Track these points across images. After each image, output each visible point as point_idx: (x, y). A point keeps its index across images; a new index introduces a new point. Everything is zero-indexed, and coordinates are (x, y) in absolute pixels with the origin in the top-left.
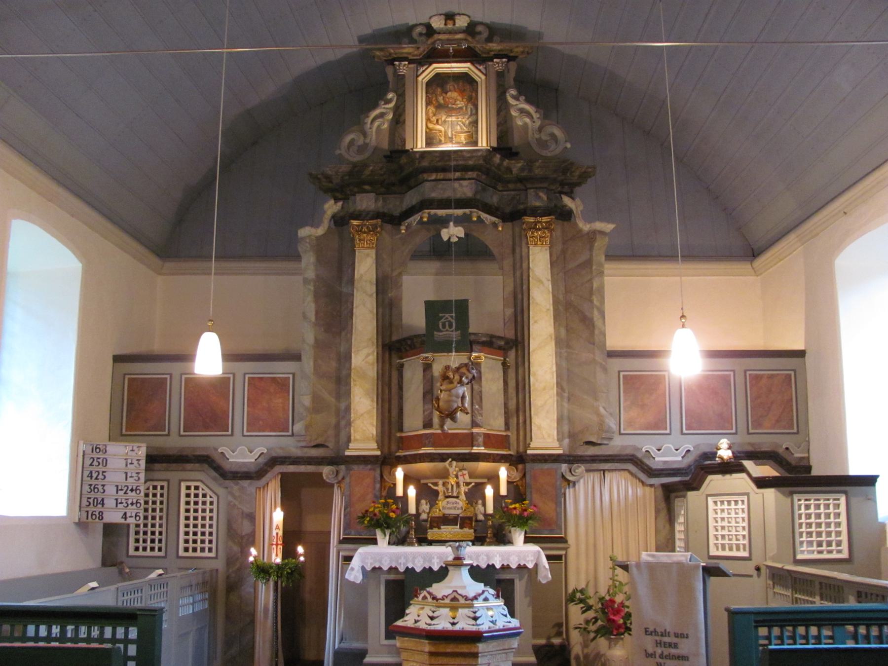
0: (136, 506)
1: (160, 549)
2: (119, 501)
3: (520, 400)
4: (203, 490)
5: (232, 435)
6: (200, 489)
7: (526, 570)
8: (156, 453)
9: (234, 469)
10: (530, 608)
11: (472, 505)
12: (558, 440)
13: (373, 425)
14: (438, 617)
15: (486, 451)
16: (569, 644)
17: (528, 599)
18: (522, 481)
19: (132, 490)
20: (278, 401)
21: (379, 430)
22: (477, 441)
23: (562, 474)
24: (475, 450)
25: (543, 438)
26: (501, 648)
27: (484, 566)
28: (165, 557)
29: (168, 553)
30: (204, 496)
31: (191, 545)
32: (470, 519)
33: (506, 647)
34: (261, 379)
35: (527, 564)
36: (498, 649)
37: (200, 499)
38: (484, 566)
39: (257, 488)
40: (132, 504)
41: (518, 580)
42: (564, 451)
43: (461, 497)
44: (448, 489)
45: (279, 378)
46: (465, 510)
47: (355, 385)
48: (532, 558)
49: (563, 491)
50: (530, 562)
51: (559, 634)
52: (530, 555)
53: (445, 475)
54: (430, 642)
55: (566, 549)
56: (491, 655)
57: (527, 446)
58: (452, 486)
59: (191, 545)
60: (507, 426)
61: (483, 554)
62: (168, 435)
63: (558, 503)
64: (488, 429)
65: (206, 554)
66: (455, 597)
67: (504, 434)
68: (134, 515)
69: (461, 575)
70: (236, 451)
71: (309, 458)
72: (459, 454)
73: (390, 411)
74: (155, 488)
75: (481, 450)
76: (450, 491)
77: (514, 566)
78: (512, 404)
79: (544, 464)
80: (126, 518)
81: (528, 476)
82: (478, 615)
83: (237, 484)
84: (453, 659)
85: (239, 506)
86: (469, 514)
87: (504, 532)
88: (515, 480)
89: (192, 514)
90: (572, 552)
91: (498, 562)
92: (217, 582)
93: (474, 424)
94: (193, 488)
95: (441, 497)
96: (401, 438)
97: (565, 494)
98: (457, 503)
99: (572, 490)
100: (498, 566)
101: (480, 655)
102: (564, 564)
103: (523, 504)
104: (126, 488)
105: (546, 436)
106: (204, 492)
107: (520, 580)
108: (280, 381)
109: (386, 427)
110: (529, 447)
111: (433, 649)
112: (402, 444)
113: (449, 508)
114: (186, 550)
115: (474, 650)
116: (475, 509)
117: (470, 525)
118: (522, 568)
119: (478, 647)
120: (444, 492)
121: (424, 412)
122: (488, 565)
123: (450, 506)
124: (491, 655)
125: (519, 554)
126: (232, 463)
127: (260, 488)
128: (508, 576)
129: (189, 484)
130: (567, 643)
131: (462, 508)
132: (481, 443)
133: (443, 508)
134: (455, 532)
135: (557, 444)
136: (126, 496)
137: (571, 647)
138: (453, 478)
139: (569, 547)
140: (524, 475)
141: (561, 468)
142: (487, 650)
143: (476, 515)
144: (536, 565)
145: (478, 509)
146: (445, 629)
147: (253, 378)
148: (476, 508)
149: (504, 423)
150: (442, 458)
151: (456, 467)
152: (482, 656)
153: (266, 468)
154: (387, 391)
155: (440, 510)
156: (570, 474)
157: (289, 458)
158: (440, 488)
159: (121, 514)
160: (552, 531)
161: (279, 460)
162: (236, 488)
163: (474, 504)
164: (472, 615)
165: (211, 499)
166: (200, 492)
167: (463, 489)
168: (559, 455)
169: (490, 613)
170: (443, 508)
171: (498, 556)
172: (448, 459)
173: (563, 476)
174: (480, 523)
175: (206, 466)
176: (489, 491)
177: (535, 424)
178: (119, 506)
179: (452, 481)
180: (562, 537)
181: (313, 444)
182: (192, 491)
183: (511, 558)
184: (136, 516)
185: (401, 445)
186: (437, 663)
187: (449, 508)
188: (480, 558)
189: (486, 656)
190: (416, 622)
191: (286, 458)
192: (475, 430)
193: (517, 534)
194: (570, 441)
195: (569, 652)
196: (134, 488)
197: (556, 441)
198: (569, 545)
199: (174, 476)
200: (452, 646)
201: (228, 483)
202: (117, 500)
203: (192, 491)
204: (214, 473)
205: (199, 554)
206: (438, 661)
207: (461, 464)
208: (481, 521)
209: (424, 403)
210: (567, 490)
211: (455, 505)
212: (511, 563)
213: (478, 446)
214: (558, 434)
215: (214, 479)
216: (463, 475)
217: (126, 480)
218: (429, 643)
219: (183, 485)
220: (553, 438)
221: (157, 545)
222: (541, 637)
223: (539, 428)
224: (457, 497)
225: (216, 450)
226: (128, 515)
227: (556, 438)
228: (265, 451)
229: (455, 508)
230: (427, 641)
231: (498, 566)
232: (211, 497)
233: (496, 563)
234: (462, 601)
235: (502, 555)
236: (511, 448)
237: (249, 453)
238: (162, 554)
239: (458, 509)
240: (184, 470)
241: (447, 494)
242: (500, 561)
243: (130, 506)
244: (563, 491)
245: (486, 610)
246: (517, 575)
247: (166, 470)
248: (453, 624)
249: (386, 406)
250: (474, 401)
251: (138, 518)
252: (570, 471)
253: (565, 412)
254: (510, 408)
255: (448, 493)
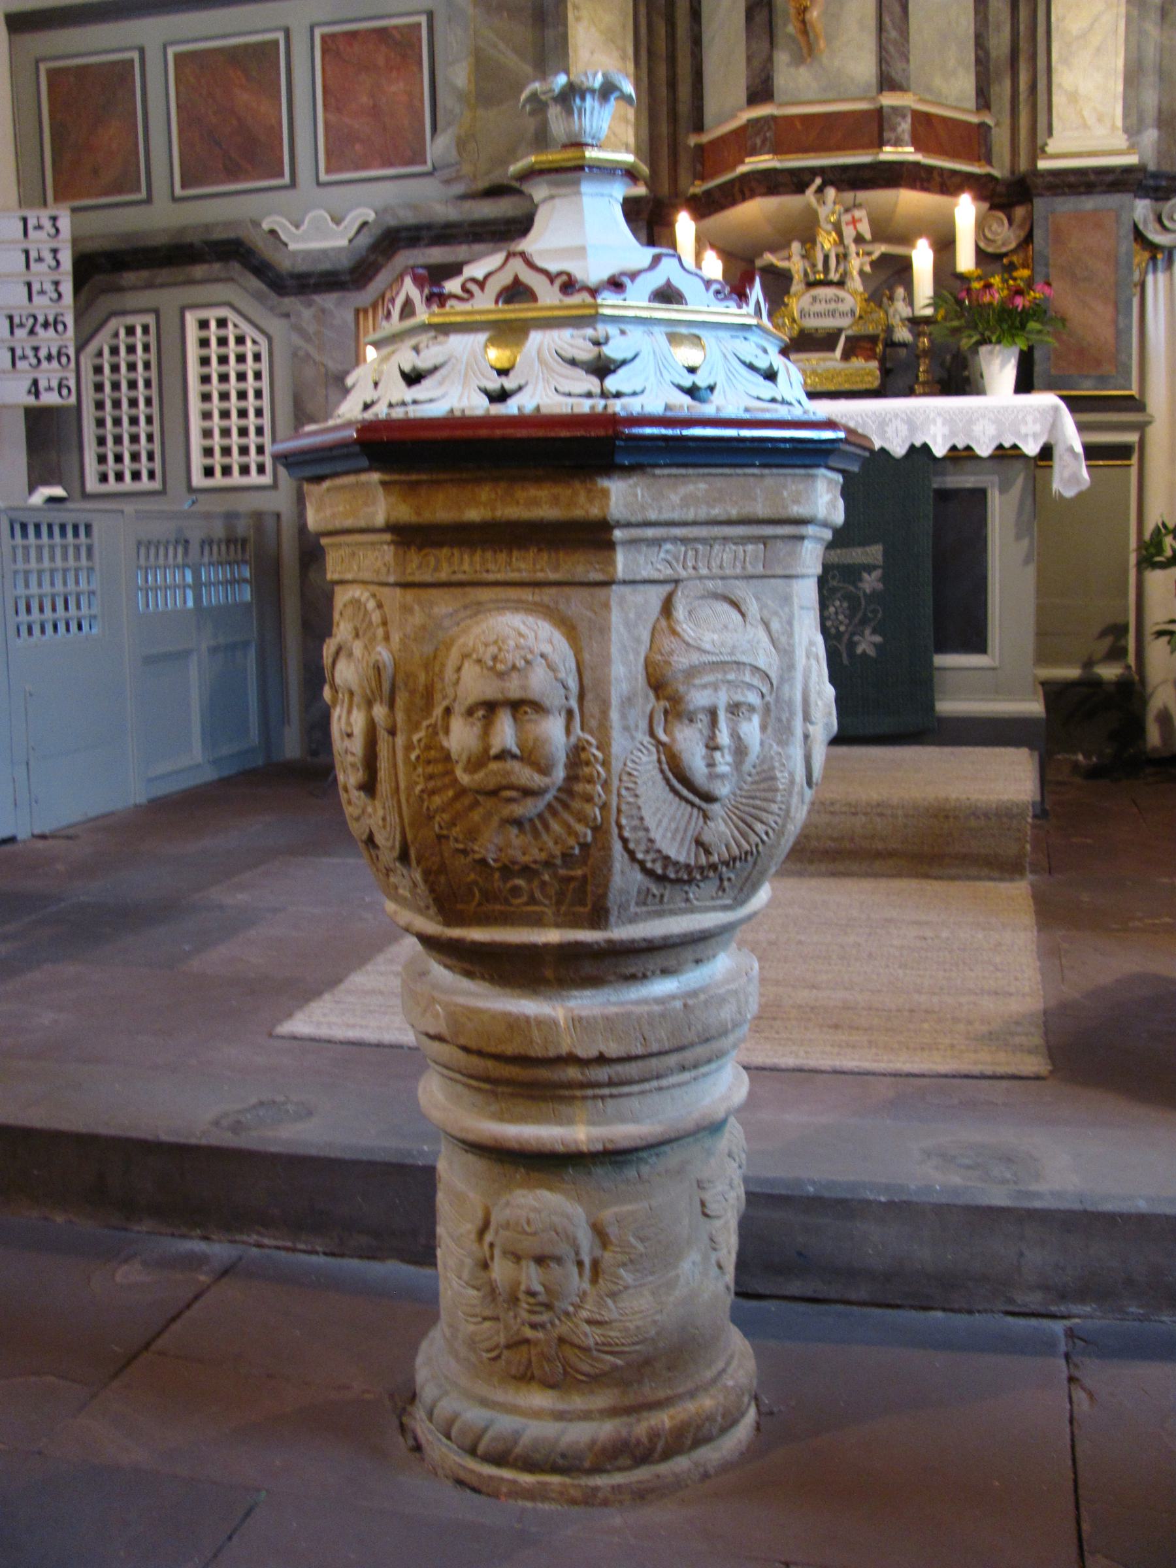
0: (59, 362)
1: (152, 475)
2: (19, 353)
3: (1022, 28)
4: (235, 326)
5: (293, 184)
6: (230, 326)
7: (1019, 465)
8: (123, 246)
9: (302, 267)
10: (1031, 570)
11: (880, 305)
12: (1126, 130)
13: (627, 121)
14: (435, 369)
15: (919, 158)
16: (1143, 681)
17: (1025, 543)
18: (1026, 251)
19: (46, 325)
20: (396, 88)
21: (645, 135)
22: (894, 129)
23: (1136, 227)
24: (889, 154)
25: (1085, 126)
26: (734, 512)
27: (899, 450)
28: (163, 492)
29: (168, 486)
30: (240, 340)
31: (218, 460)
32: (873, 339)
33: (761, 509)
34: (353, 35)
35: (1020, 445)
36: (717, 512)
37: (232, 349)
38: (899, 450)
39: (357, 312)
40: (49, 358)
41: (997, 493)
42: (1140, 158)
43: (849, 284)
44: (814, 266)
45: (396, 27)
46: (861, 317)
47: (578, 19)
48: (1037, 428)
49: (1136, 276)
50: (1031, 440)
51: (1116, 654)
52: (1029, 419)
53: (807, 233)
54: (387, 478)
55: (1141, 427)
56: (684, 541)
57: (1037, 151)
58: (826, 258)
59: (218, 460)
60: (983, 99)
61: (896, 416)
62: (149, 200)
63: (1120, 308)
64: (922, 101)
65: (254, 478)
66: (517, 281)
67: (974, 119)
68: (55, 384)
69: (580, 211)
70: (303, 222)
71: (474, 224)
72: (845, 168)
73: (672, 85)
74: (130, 331)
75: (907, 153)
76: (820, 267)
77: (984, 450)
78: (1000, 43)
79: (1083, 198)
80: (37, 395)
81: (1038, 234)
82: (613, 351)
83: (310, 305)
84: (502, 557)
85: (317, 358)
86: (871, 329)
87: (966, 373)
88: (1004, 250)
89: (215, 387)
90: (1158, 436)
91: (939, 440)
92: (279, 545)
93: (887, 83)
94: (213, 324)
95: (797, 286)
96: (700, 148)
97: (1143, 285)
98: (838, 300)
99: (1161, 277)
100: (939, 451)
101: (618, 534)
102: (1134, 471)
103: (1015, 279)
104: (31, 321)
105: (1091, 121)
106: (238, 332)
107: (1001, 492)
108: (398, 36)
109: (664, 129)
110: (1043, 151)
111: (405, 513)
112: (703, 165)
113: (818, 315)
114: (209, 472)
115: (585, 509)
116: (887, 313)
117: (870, 353)
118: (1006, 455)
119: (605, 493)
120: (806, 274)
121: (749, 59)
122: (912, 447)
123: (818, 307)
124: (684, 541)
125: (999, 416)
126: (295, 254)
127: (366, 311)
128: (966, 480)
129: (203, 314)
130: (1137, 678)
131: (853, 312)
132: (907, 137)
133: (803, 314)
134: (827, 370)
135: (1121, 141)
136: (34, 341)
137: (1149, 690)
138: (829, 233)
139: (1148, 423)
140: (1029, 239)
141: (1132, 209)
142: (653, 516)
143: (889, 329)
144: (1047, 452)
145: (896, 311)
146: (458, 414)
147: (333, 36)
148: (891, 311)
149: (973, 93)
150: (797, 182)
151: (835, 203)
152: (633, 542)
153: (372, 258)
154: (661, 29)
155: (794, 320)
156: (1158, 227)
157: (429, 227)
158: (796, 265)
159: (27, 383)
160: (1103, 381)
161: (404, 234)
162: (307, 314)
163: (885, 300)
164: (586, 352)
165: (256, 348)
166: (231, 333)
167: (855, 264)
168: (1127, 170)
169: (688, 355)
170: (803, 314)
171: (939, 421)
172: (813, 181)
173: (1139, 236)
174: (903, 352)
175: (236, 267)
176: (922, 257)
177: (1060, 85)
178: (20, 364)
179: (826, 242)
180: (1131, 397)
181: (482, 184)
182: (213, 331)
183: (977, 429)
184: (60, 386)
185: (699, 167)
186: (428, 578)
187: (818, 315)
188: (890, 431)
189: (657, 542)
190: (367, 407)
191: (418, 228)
192: (889, 100)
193: (997, 362)
194: (1159, 137)
195: (1144, 701)
196: (51, 319)
197: (1120, 132)
198: (1152, 416)
199: (167, 298)
200: (485, 493)
201: (290, 303)
202: (13, 350)
203: (213, 331)
204: (255, 283)
205: (236, 479)
206: (436, 569)
207: (849, 196)
208: (904, 345)
209: (748, 38)
210: (1150, 279)
211: (833, 306)
212: (978, 442)
213: (897, 143)
214: (1126, 116)
215: (258, 297)
216: (854, 222)
217: (30, 299)
218: (384, 484)
219: (191, 319)
220: (1113, 127)
221: (144, 465)
222: (1067, 661)
223: (1073, 97)
224: (841, 284)
225: (256, 224)
226: (43, 384)
227: (1119, 123)
228: (371, 216)
229: (832, 313)
230: (375, 477)
231: (939, 451)
232: (254, 342)
233: (935, 443)
234: (548, 296)
235: (949, 419)
236: (994, 161)
237: (334, 226)
238: (156, 485)
239: (843, 315)
240: (191, 282)
241: (811, 278)
242: (944, 436)
243: (45, 364)
244: (1136, 276)
245: (663, 340)
246: (996, 479)
247: (150, 285)
248: (501, 396)
249: (662, 70)
250: (887, 19)
251: (65, 392)
252: (1159, 220)
253: (1151, 53)
254: (994, 54)
255: (815, 273)
